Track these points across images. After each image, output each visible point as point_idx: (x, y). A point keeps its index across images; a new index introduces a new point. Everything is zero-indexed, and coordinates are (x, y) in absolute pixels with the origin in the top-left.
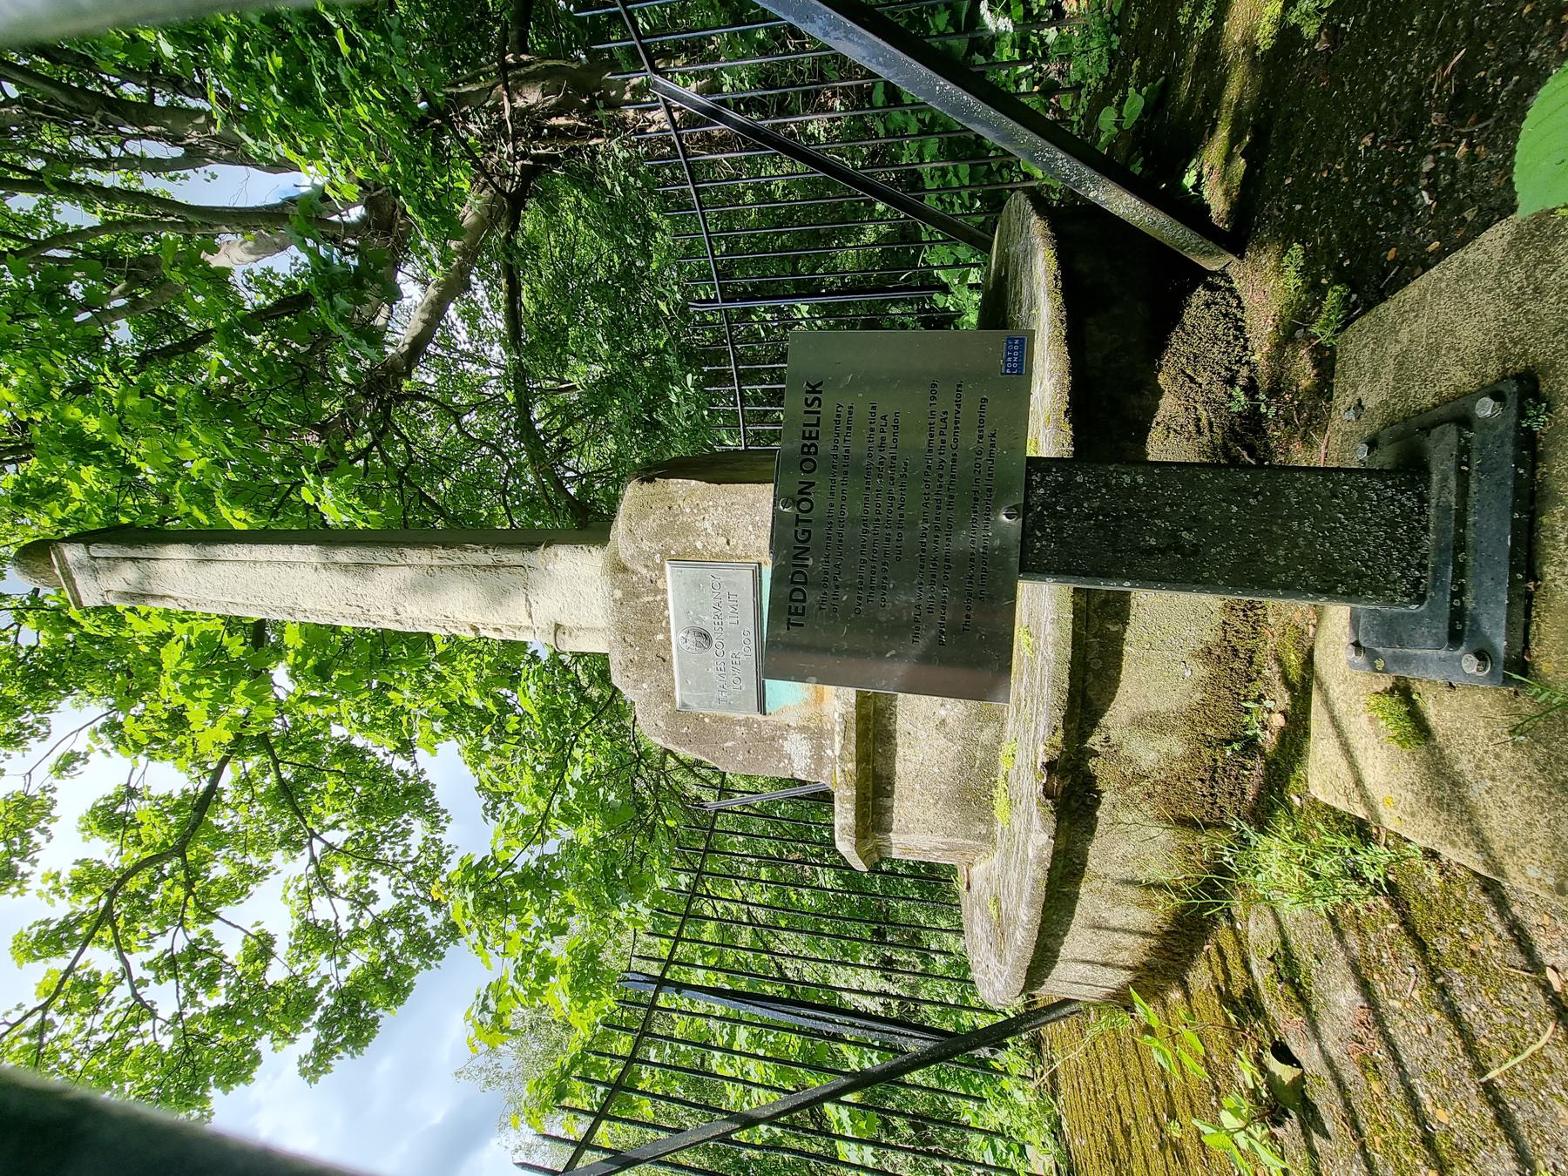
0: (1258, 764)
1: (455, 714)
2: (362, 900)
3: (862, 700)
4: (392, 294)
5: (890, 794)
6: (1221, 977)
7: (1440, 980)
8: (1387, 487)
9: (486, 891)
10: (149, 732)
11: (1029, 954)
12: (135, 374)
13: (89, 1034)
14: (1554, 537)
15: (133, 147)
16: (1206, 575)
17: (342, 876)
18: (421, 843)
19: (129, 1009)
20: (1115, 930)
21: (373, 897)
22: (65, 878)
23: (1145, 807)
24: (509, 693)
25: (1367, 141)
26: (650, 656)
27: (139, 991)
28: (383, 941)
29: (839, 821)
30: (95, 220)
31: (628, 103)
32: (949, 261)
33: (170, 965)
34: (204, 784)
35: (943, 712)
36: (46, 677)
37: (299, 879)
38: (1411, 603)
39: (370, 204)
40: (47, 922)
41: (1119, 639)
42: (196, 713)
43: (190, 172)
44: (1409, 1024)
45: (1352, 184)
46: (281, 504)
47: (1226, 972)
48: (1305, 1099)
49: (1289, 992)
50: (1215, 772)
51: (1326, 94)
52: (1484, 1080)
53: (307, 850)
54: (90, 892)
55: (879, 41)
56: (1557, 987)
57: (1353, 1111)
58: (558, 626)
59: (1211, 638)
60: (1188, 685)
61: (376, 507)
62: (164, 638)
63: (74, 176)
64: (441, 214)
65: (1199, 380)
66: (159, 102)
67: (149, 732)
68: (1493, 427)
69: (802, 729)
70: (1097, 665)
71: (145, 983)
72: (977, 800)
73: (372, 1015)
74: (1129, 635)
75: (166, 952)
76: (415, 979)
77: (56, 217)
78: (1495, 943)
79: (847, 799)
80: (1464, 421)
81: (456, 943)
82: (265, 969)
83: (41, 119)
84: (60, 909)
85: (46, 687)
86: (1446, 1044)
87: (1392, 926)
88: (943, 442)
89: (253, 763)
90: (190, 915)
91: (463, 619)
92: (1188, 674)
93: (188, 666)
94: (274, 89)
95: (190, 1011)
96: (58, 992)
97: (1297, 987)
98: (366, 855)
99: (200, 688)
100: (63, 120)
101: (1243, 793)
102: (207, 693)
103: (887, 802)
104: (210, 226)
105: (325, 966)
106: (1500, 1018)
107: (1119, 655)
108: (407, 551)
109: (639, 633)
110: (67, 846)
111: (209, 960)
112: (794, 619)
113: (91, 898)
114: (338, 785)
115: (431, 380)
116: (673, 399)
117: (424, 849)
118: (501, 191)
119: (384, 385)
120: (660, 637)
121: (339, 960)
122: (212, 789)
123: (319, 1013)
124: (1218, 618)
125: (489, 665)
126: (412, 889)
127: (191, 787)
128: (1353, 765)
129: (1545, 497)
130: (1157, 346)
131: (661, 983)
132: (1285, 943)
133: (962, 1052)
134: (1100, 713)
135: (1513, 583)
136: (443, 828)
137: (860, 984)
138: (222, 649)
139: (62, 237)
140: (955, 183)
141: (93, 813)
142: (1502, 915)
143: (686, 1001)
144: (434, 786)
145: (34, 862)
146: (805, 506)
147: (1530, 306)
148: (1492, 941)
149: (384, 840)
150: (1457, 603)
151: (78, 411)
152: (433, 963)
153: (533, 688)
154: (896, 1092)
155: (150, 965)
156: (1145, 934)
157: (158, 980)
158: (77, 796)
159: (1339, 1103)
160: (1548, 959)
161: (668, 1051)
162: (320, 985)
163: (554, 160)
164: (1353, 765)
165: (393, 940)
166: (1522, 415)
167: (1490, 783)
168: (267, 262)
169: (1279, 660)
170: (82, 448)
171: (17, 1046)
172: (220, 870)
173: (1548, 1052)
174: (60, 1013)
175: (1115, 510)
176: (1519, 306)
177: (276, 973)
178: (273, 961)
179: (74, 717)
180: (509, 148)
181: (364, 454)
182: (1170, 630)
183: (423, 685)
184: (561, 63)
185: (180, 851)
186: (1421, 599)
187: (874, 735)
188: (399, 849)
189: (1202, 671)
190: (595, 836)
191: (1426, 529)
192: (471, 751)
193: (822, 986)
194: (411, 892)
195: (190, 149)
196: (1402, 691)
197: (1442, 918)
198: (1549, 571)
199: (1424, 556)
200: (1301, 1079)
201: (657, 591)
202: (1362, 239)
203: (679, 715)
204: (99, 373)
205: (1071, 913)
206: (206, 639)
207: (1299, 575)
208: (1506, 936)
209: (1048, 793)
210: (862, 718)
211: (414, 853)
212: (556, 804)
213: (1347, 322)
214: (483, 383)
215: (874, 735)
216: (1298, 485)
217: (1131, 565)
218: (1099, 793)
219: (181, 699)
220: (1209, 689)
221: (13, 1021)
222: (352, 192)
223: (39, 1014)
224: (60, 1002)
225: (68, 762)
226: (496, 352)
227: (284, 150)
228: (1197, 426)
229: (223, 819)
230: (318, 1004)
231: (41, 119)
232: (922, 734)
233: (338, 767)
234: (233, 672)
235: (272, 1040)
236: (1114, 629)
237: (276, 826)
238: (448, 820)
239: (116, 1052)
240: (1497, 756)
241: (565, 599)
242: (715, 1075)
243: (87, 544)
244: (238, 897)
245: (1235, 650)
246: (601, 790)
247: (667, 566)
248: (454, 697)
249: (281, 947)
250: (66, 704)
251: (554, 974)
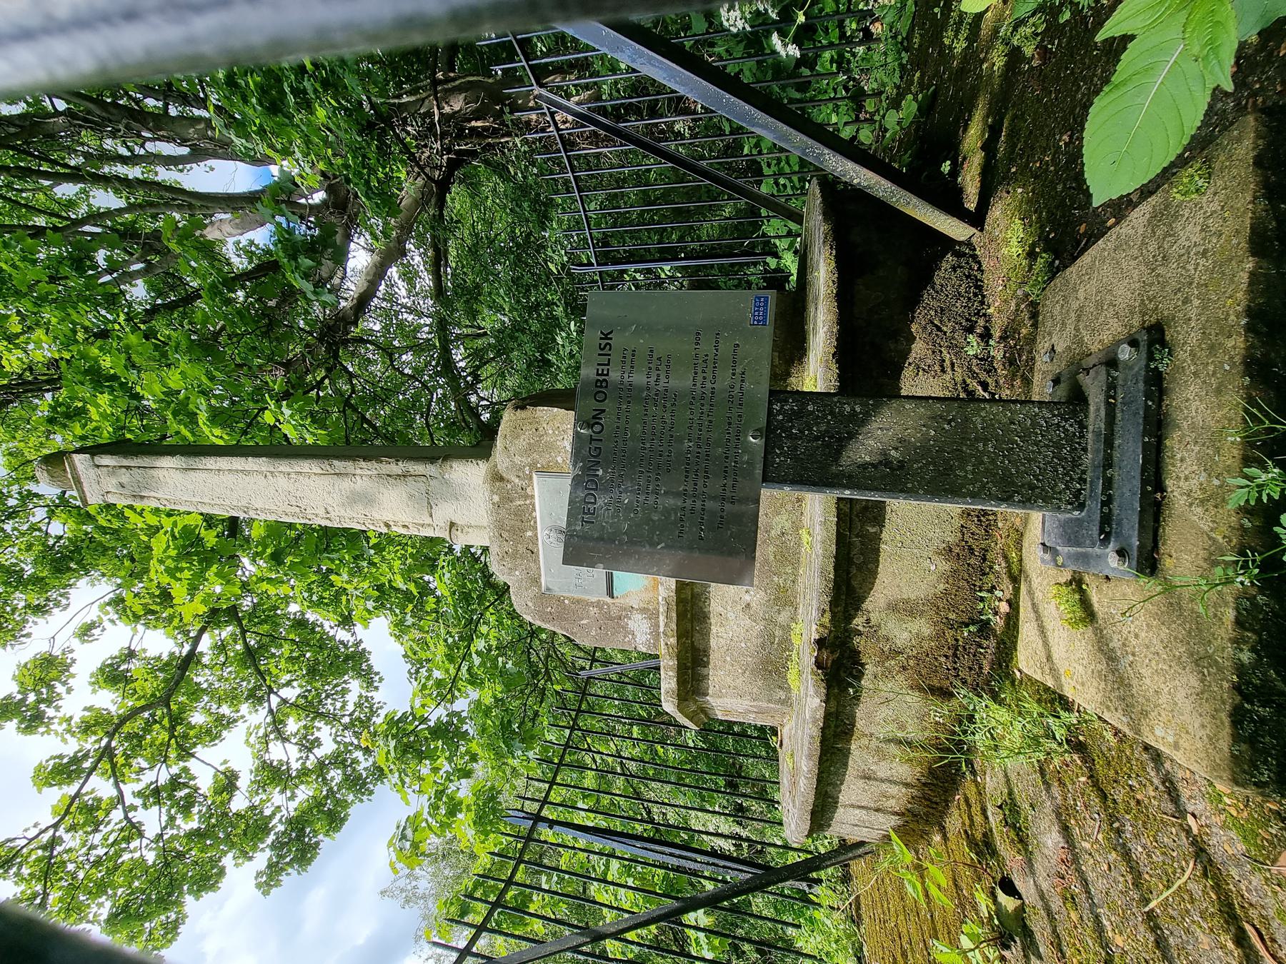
0: (992, 643)
1: (383, 594)
2: (309, 745)
3: (680, 587)
4: (340, 257)
5: (706, 665)
6: (967, 822)
7: (1116, 825)
8: (1054, 415)
9: (405, 740)
10: (145, 605)
11: (811, 799)
12: (144, 322)
13: (89, 849)
14: (1173, 457)
15: (149, 146)
16: (909, 485)
17: (292, 725)
18: (357, 699)
19: (122, 830)
20: (882, 781)
21: (317, 742)
22: (76, 719)
23: (900, 678)
24: (431, 579)
25: (1066, 138)
26: (521, 549)
27: (130, 815)
28: (324, 779)
29: (664, 686)
30: (121, 203)
31: (532, 109)
32: (784, 232)
33: (154, 795)
34: (187, 648)
35: (747, 598)
36: (64, 562)
37: (258, 727)
38: (1074, 509)
39: (330, 190)
40: (61, 757)
41: (877, 538)
42: (179, 591)
43: (194, 165)
44: (1097, 863)
45: (1056, 172)
46: (249, 425)
47: (971, 818)
48: (1025, 927)
49: (1012, 834)
50: (957, 649)
51: (1039, 100)
52: (1147, 909)
53: (266, 704)
54: (95, 733)
55: (674, 65)
56: (1195, 831)
57: (1058, 936)
58: (452, 525)
59: (952, 539)
60: (934, 577)
61: (324, 427)
62: (154, 531)
63: (106, 170)
64: (386, 200)
65: (945, 329)
66: (173, 111)
67: (145, 605)
68: (1131, 368)
69: (643, 610)
70: (858, 559)
71: (135, 808)
72: (777, 671)
73: (314, 840)
74: (885, 536)
75: (152, 783)
76: (350, 811)
77: (92, 201)
78: (1153, 794)
80: (1111, 363)
81: (382, 783)
82: (229, 800)
83: (81, 126)
84: (71, 747)
85: (69, 569)
86: (1121, 879)
87: (1083, 779)
89: (227, 631)
90: (173, 754)
91: (378, 517)
92: (933, 568)
93: (173, 553)
94: (254, 100)
95: (170, 832)
96: (67, 812)
97: (1018, 830)
98: (311, 708)
99: (182, 570)
100: (97, 128)
101: (981, 668)
102: (187, 574)
103: (704, 671)
104: (208, 208)
105: (278, 798)
106: (1158, 858)
107: (877, 551)
108: (336, 462)
109: (512, 530)
110: (82, 696)
111: (187, 791)
113: (94, 738)
114: (292, 651)
115: (377, 327)
116: (559, 341)
117: (359, 705)
118: (430, 179)
119: (337, 333)
120: (529, 533)
121: (289, 794)
122: (192, 654)
123: (272, 837)
124: (957, 523)
125: (412, 555)
126: (349, 737)
127: (177, 650)
128: (1046, 644)
129: (1168, 425)
130: (912, 301)
131: (537, 818)
132: (1010, 793)
133: (775, 883)
134: (862, 599)
135: (1144, 493)
136: (377, 688)
137: (713, 825)
138: (199, 539)
139: (95, 217)
140: (787, 170)
141: (101, 670)
142: (1158, 771)
143: (570, 837)
144: (370, 653)
145: (58, 708)
146: (597, 428)
147: (1160, 270)
148: (1150, 793)
149: (327, 697)
150: (1106, 510)
151: (97, 351)
152: (365, 798)
153: (448, 575)
154: (744, 921)
155: (139, 794)
156: (907, 785)
157: (145, 806)
158: (89, 658)
159: (1049, 930)
160: (1190, 808)
161: (555, 878)
162: (274, 814)
163: (473, 154)
164: (1046, 644)
165: (333, 779)
166: (1151, 358)
167: (1131, 658)
168: (250, 235)
169: (1005, 557)
170: (99, 379)
171: (34, 857)
172: (198, 718)
173: (1190, 886)
174: (68, 831)
176: (1153, 270)
177: (239, 803)
178: (237, 792)
179: (88, 594)
180: (438, 145)
181: (319, 385)
182: (917, 532)
183: (360, 569)
184: (480, 78)
185: (166, 702)
186: (1081, 506)
187: (690, 616)
188: (339, 705)
189: (944, 566)
190: (495, 697)
191: (1085, 450)
192: (396, 625)
193: (682, 828)
194: (347, 740)
195: (194, 148)
196: (1077, 583)
197: (1117, 773)
198: (1169, 483)
199: (1084, 472)
200: (1021, 909)
201: (527, 497)
202: (1063, 216)
203: (545, 597)
204: (115, 321)
205: (846, 765)
206: (188, 532)
207: (983, 487)
208: (1161, 788)
209: (819, 664)
210: (681, 601)
211: (350, 707)
212: (464, 669)
213: (1051, 279)
214: (418, 329)
215: (690, 616)
216: (983, 414)
218: (863, 665)
219: (165, 579)
220: (951, 581)
221: (30, 837)
222: (314, 180)
223: (51, 832)
224: (69, 820)
225: (86, 632)
226: (427, 304)
227: (262, 148)
228: (942, 366)
229: (201, 678)
230: (271, 829)
231: (81, 126)
232: (731, 615)
233: (292, 636)
234: (207, 558)
235: (234, 858)
236: (872, 530)
237: (244, 684)
238: (381, 680)
239: (111, 865)
240: (1137, 636)
241: (459, 504)
242: (595, 902)
243: (93, 455)
244: (212, 740)
245: (971, 549)
246: (500, 659)
247: (535, 476)
248: (384, 580)
249: (244, 782)
250: (83, 582)
251: (460, 811)
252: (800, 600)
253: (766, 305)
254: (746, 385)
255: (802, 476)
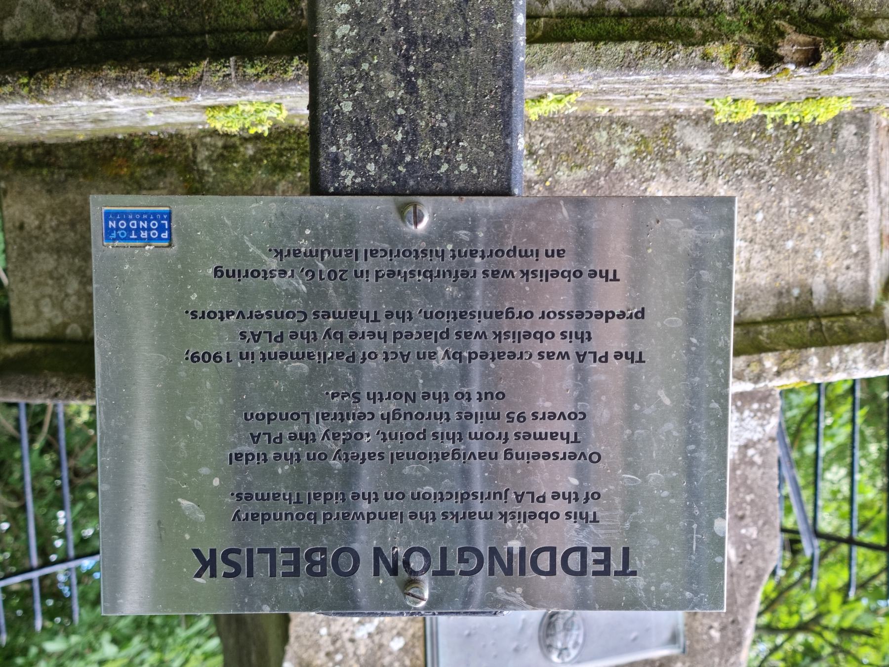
29: (862, 372)
79: (825, 359)
88: (294, 335)
112: (616, 565)
146: (417, 562)
175: (397, 47)
217: (489, 15)
252: (660, 109)
253: (124, 216)
254: (304, 245)
255: (494, 115)
